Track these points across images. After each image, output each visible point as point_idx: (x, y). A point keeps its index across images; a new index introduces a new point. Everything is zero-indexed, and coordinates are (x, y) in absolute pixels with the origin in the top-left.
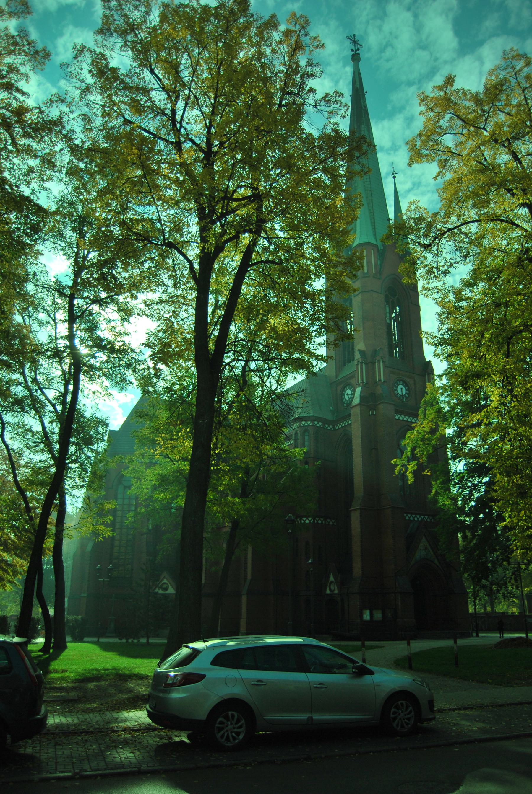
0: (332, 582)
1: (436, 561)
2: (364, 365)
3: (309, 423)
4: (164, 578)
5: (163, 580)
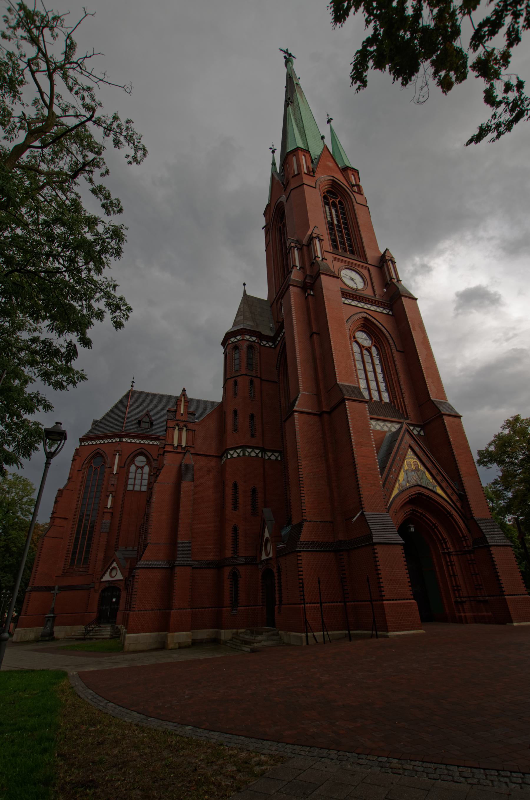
1: (439, 491)
3: (238, 337)
4: (114, 561)
5: (112, 563)
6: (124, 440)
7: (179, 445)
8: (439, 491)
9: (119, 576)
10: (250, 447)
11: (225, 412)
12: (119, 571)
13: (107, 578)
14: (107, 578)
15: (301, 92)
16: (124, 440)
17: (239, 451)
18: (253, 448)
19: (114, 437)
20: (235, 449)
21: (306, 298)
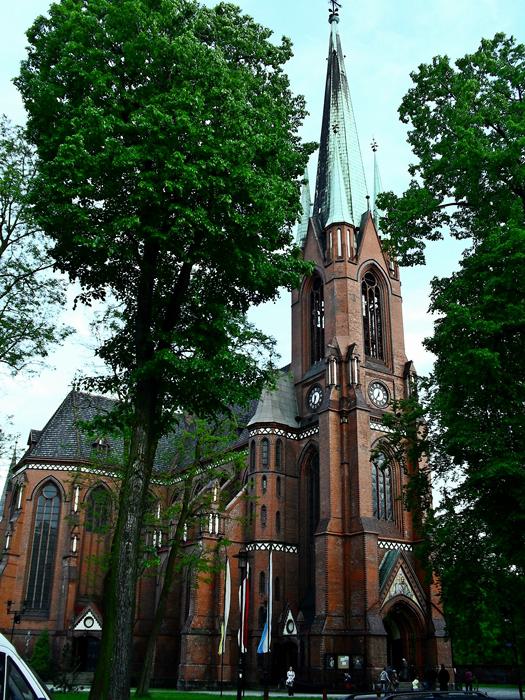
0: (290, 621)
1: (414, 599)
2: (217, 520)
3: (268, 430)
4: (89, 610)
6: (83, 470)
7: (214, 532)
8: (414, 599)
9: (97, 627)
10: (275, 542)
11: (252, 504)
12: (95, 622)
13: (80, 626)
14: (80, 626)
15: (346, 87)
16: (83, 470)
17: (266, 545)
18: (278, 543)
19: (71, 464)
20: (263, 542)
21: (341, 424)
